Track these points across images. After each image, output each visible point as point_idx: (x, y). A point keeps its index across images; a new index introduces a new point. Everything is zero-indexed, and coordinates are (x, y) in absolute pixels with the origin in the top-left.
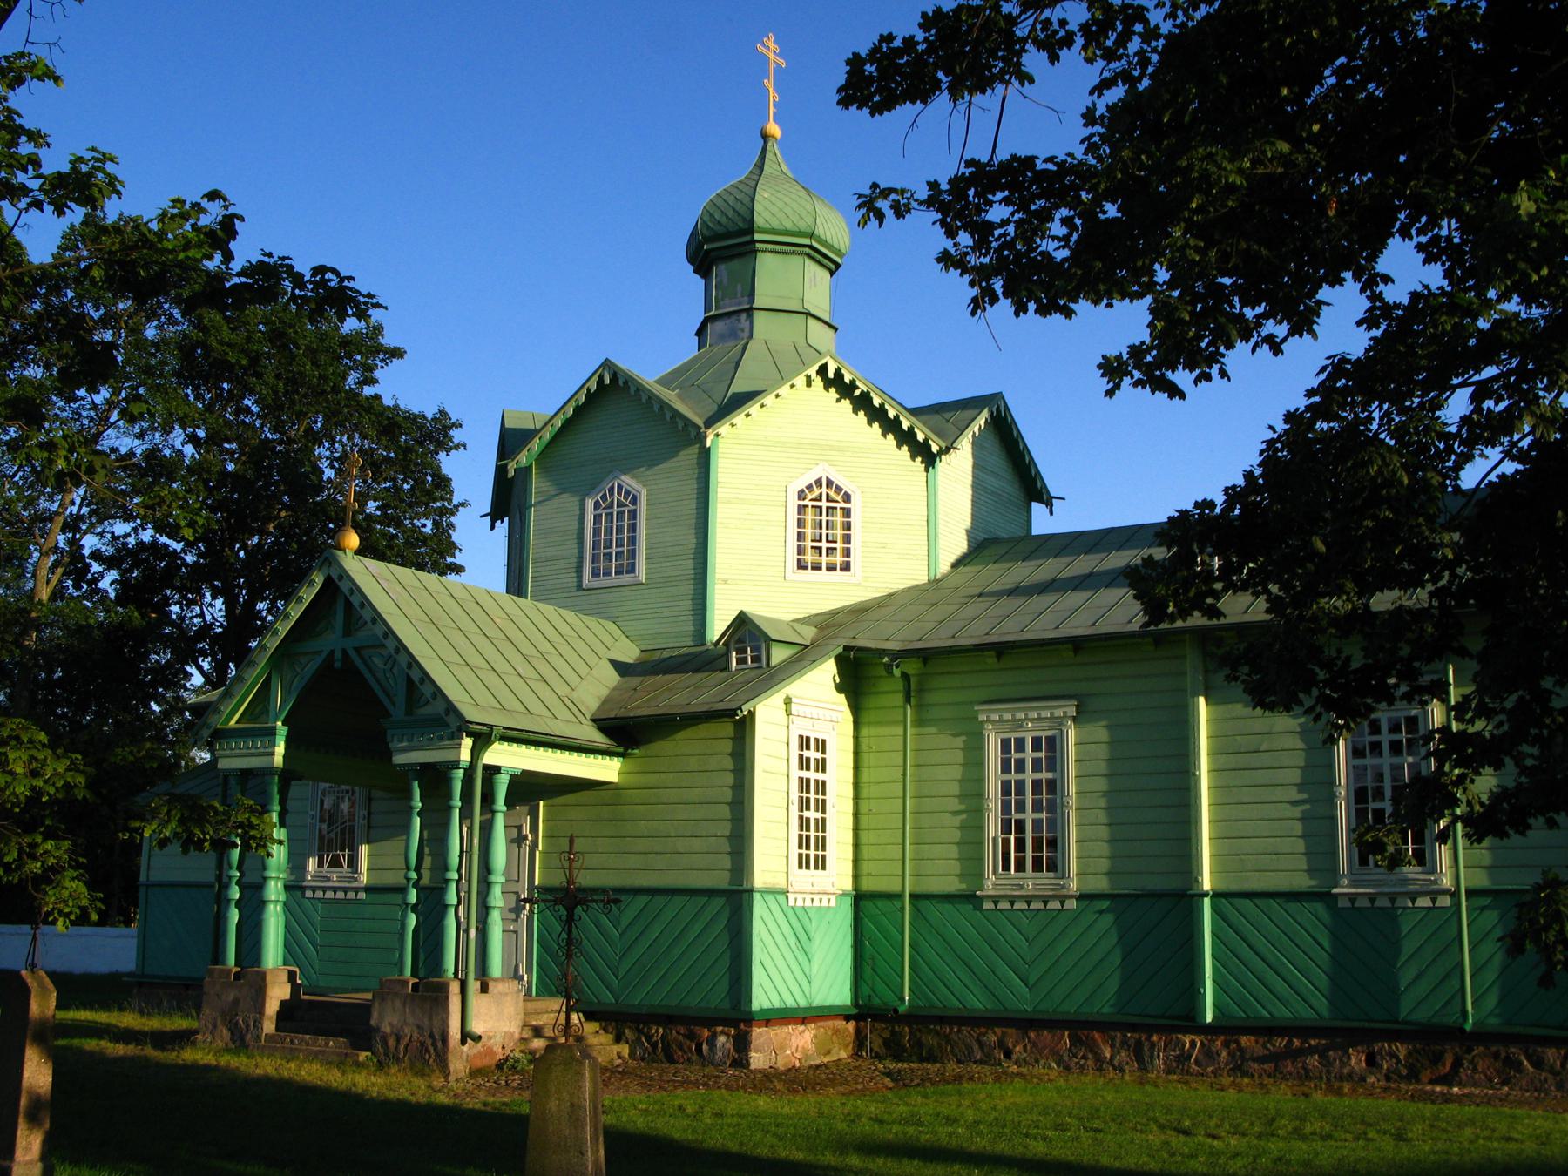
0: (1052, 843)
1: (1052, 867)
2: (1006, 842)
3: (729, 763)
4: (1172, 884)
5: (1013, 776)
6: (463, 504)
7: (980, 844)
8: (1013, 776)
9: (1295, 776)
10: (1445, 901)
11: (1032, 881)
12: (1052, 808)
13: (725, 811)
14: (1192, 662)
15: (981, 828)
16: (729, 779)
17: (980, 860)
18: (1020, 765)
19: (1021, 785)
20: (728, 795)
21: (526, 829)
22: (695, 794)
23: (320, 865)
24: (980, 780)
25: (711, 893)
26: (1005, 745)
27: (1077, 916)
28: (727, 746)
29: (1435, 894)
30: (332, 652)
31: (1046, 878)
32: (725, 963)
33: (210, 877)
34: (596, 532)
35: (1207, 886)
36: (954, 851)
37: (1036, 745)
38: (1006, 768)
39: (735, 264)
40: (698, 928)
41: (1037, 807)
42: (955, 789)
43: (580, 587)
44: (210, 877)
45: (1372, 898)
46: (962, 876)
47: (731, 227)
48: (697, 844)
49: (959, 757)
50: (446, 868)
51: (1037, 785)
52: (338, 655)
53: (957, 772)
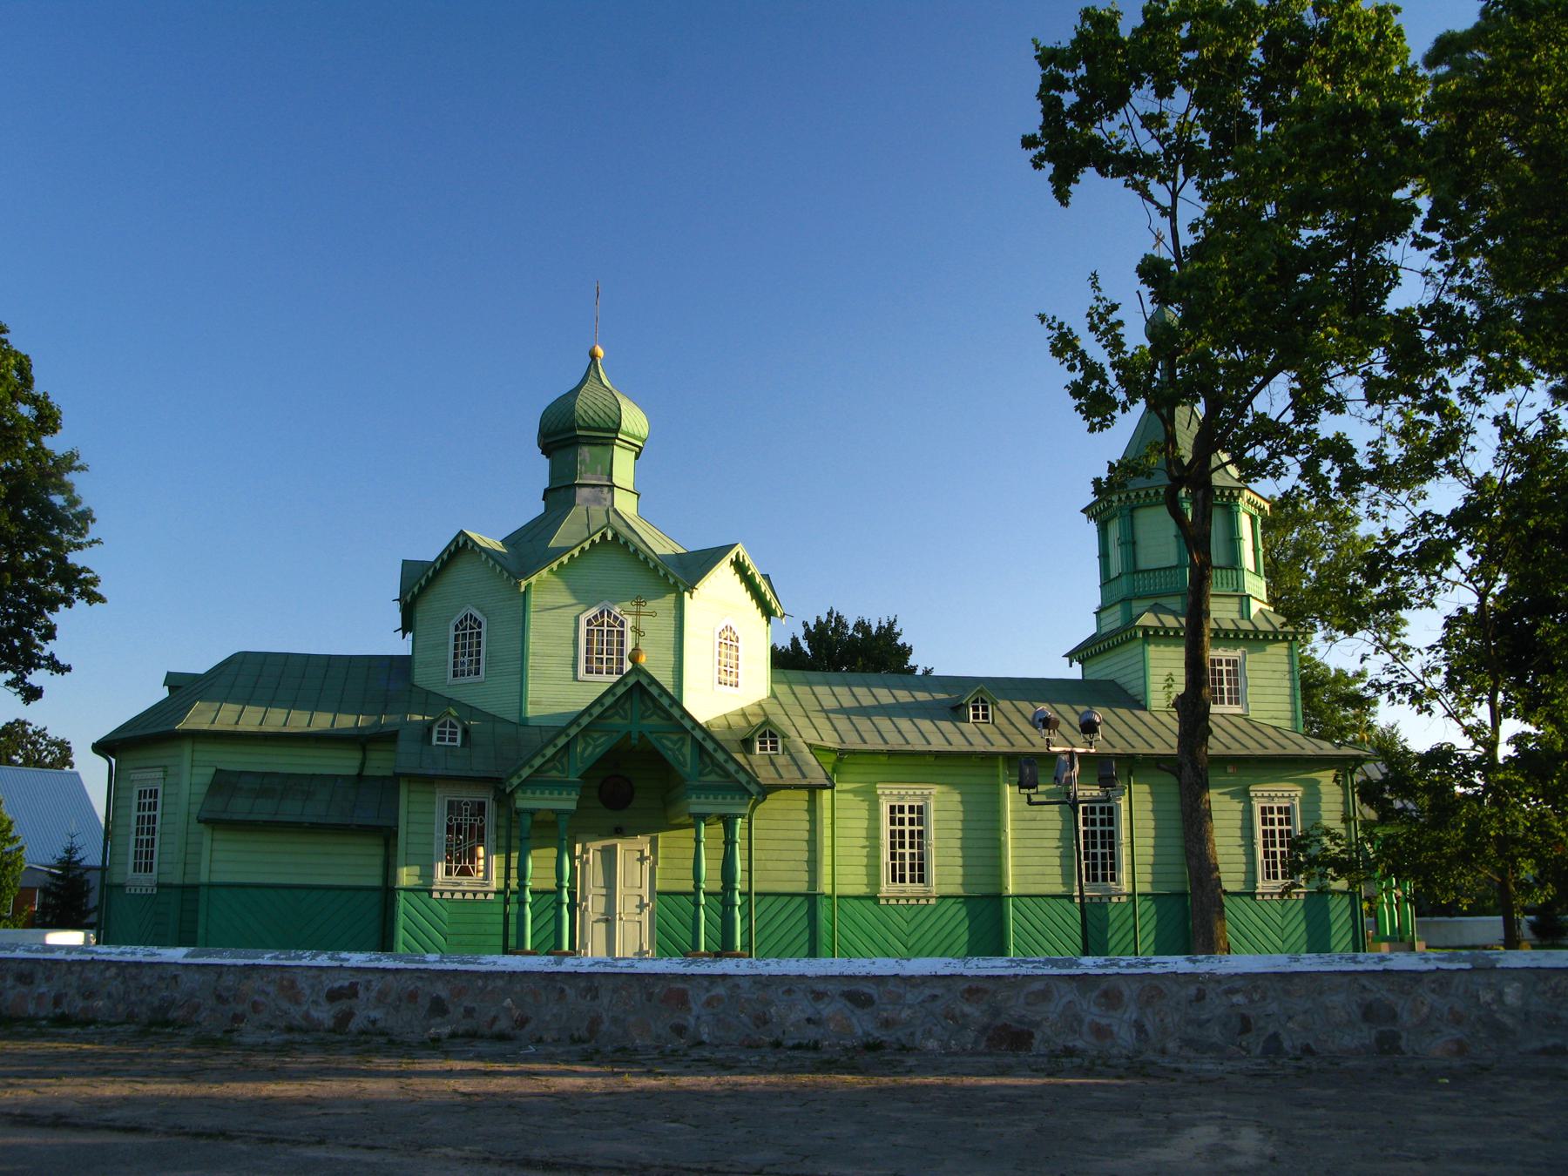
0: (921, 867)
1: (921, 880)
2: (894, 866)
3: (806, 816)
4: (990, 890)
5: (897, 828)
6: (98, 541)
7: (878, 867)
8: (897, 828)
9: (1057, 834)
10: (1124, 899)
11: (909, 887)
12: (920, 846)
13: (804, 846)
14: (1002, 770)
15: (878, 857)
16: (806, 826)
17: (878, 876)
18: (902, 822)
19: (902, 833)
20: (806, 836)
21: (647, 853)
22: (780, 834)
23: (448, 872)
24: (878, 829)
25: (793, 895)
26: (892, 808)
27: (936, 907)
28: (805, 805)
29: (1119, 895)
30: (629, 733)
31: (918, 887)
32: (806, 936)
33: (691, 889)
34: (589, 642)
35: (1011, 890)
36: (863, 870)
37: (911, 809)
38: (892, 822)
39: (596, 450)
40: (783, 916)
41: (912, 846)
42: (864, 833)
43: (575, 678)
44: (691, 889)
45: (1100, 898)
46: (867, 885)
47: (602, 425)
48: (782, 865)
49: (865, 814)
50: (734, 881)
51: (912, 833)
52: (635, 735)
53: (865, 824)
